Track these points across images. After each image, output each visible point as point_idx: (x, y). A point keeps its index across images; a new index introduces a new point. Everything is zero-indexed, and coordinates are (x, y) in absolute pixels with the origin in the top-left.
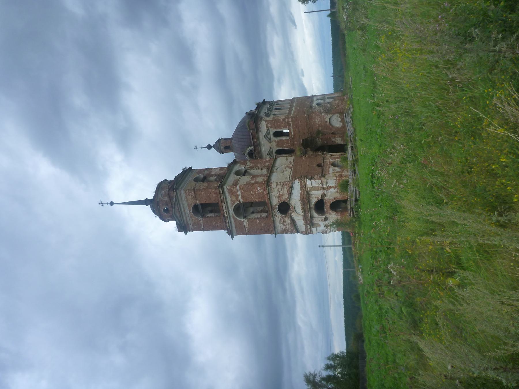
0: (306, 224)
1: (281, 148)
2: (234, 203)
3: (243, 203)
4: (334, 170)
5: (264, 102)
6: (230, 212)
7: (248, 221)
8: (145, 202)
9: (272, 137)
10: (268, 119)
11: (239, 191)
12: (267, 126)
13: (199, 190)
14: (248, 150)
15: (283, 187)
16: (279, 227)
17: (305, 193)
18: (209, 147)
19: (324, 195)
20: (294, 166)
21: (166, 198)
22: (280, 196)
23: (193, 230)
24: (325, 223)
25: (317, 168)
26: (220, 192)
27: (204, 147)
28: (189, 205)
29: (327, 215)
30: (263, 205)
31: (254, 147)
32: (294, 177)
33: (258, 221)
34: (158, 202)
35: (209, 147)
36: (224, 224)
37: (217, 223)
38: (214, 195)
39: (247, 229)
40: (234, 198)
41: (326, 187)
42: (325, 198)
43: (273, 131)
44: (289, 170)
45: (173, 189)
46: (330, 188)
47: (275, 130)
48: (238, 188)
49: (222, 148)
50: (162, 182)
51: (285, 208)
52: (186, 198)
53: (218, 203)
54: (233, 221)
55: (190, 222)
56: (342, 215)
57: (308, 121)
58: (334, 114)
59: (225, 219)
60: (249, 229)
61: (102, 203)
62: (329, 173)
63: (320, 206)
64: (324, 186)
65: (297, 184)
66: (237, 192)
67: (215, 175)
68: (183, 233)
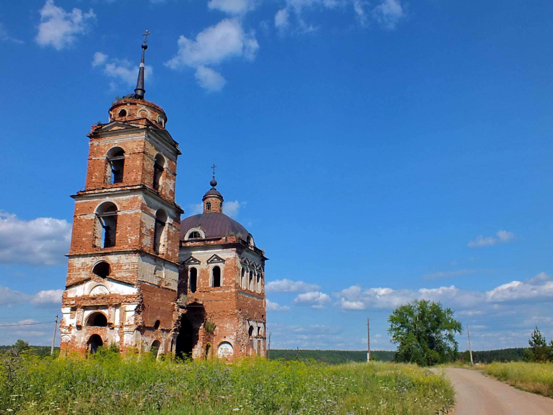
0: (77, 299)
1: (198, 275)
2: (119, 203)
5: (264, 259)
7: (92, 220)
12: (228, 259)
15: (131, 272)
24: (75, 325)
25: (154, 321)
28: (124, 144)
29: (84, 330)
33: (90, 233)
36: (94, 188)
39: (82, 217)
40: (125, 204)
45: (148, 126)
46: (121, 337)
48: (137, 211)
50: (165, 114)
52: (135, 141)
53: (121, 182)
56: (81, 350)
57: (228, 314)
63: (98, 320)
64: (125, 329)
65: (133, 291)
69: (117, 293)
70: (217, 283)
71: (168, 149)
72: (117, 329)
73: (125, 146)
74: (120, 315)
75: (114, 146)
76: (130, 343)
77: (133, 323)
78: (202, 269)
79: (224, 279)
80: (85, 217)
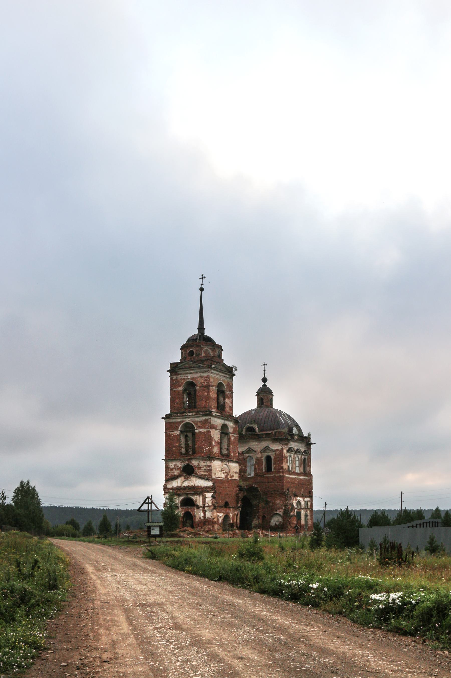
2: (195, 424)
3: (195, 432)
4: (220, 517)
6: (187, 419)
8: (201, 328)
9: (266, 454)
10: (285, 451)
11: (205, 430)
12: (277, 450)
13: (209, 391)
14: (256, 427)
15: (207, 472)
16: (172, 465)
17: (201, 491)
18: (264, 380)
19: (198, 507)
20: (228, 481)
21: (203, 354)
22: (199, 467)
23: (171, 379)
25: (224, 502)
26: (206, 412)
27: (264, 374)
30: (191, 451)
31: (258, 435)
32: (216, 482)
33: (177, 444)
34: (200, 346)
35: (264, 380)
37: (177, 404)
38: (203, 405)
39: (171, 433)
40: (199, 425)
41: (206, 509)
42: (195, 508)
43: (272, 455)
44: (223, 476)
46: (205, 513)
47: (272, 457)
49: (261, 396)
51: (189, 471)
52: (202, 377)
54: (179, 420)
55: (179, 377)
58: (283, 518)
59: (181, 413)
60: (170, 435)
61: (202, 278)
62: (217, 512)
64: (206, 508)
65: (209, 484)
66: (205, 428)
67: (224, 403)
68: (169, 368)
69: (199, 485)
70: (269, 469)
71: (226, 375)
72: (201, 508)
73: (195, 380)
74: (203, 500)
75: (187, 380)
76: (210, 517)
77: (211, 504)
78: (257, 457)
79: (275, 466)
80: (173, 433)
